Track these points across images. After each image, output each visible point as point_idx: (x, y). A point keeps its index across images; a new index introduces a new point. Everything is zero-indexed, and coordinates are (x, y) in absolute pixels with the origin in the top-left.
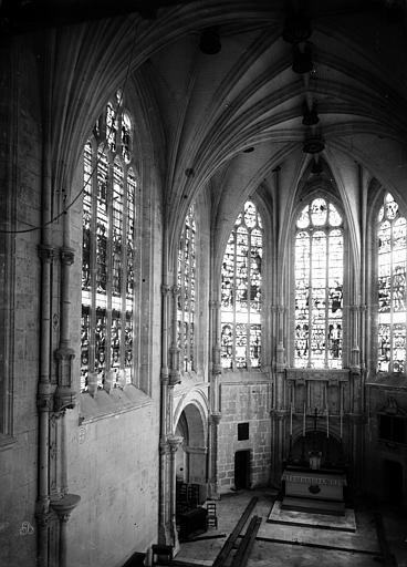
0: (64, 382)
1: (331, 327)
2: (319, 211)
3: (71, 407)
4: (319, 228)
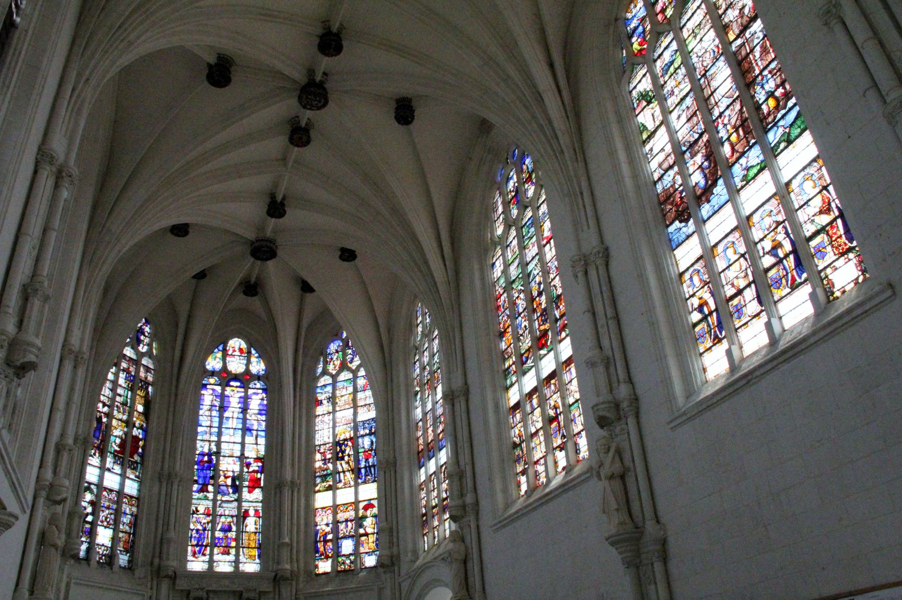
0: (164, 556)
1: (246, 512)
2: (237, 353)
3: (617, 510)
4: (236, 378)
